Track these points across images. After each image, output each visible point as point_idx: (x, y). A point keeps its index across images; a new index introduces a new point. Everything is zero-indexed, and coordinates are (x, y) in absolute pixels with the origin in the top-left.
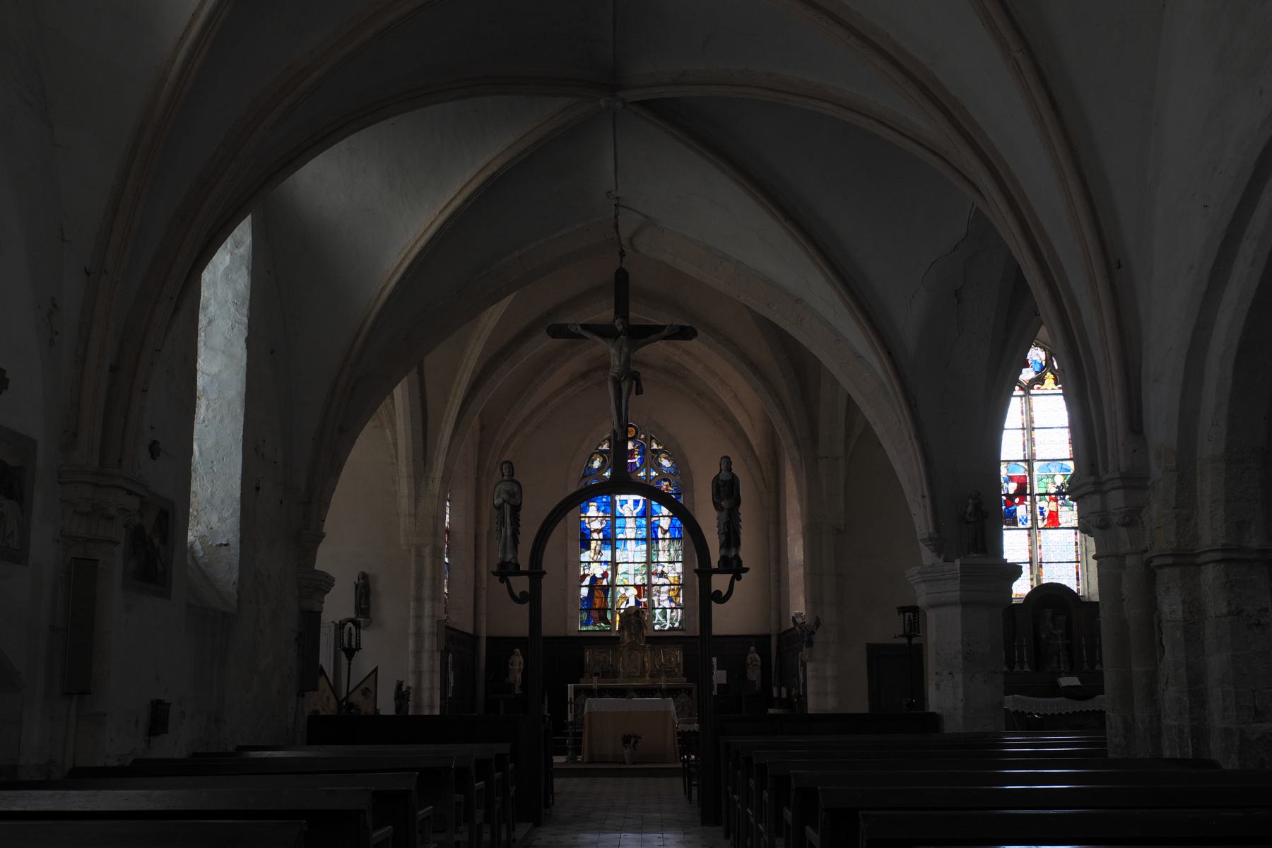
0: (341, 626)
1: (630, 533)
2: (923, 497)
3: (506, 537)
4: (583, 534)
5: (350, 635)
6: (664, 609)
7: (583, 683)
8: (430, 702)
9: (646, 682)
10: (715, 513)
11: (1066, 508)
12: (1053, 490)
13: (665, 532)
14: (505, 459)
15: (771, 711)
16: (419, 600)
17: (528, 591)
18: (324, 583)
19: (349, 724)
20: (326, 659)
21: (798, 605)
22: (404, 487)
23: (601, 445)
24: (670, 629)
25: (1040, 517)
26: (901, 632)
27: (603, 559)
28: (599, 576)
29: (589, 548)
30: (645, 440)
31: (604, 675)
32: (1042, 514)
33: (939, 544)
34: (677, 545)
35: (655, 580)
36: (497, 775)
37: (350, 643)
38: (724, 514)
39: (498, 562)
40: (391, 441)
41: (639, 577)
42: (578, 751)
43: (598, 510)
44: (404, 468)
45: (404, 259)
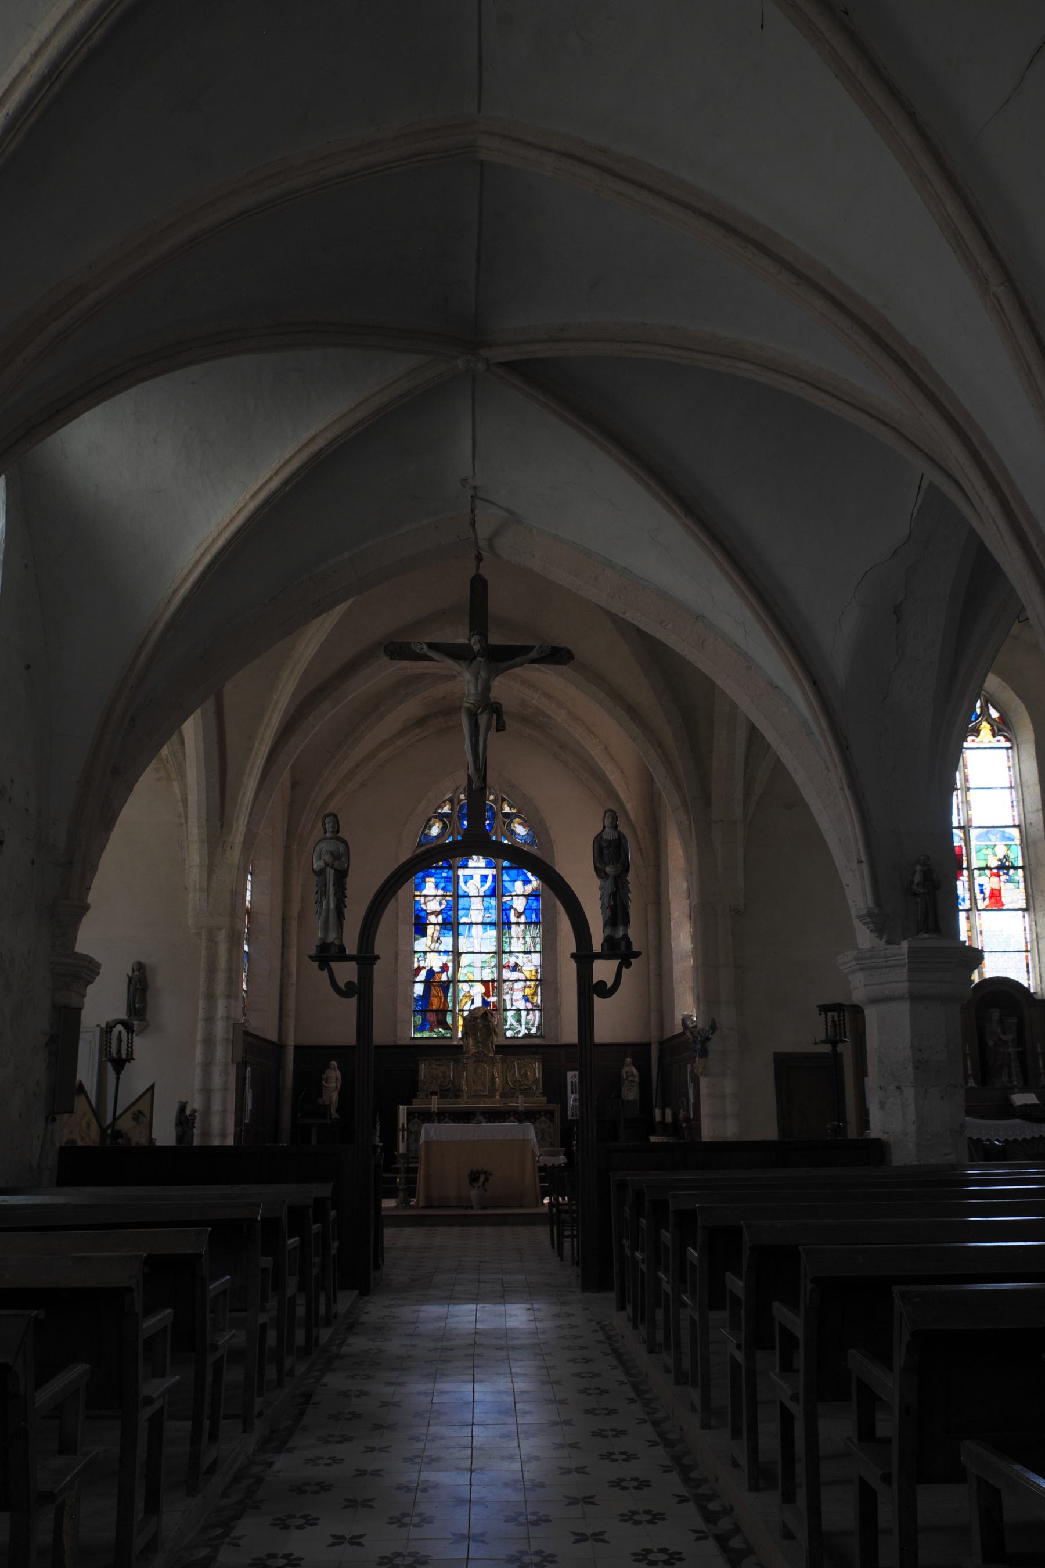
0: (109, 1028)
1: (476, 916)
2: (860, 862)
3: (328, 910)
4: (417, 917)
5: (120, 1040)
6: (518, 1010)
7: (417, 1105)
8: (221, 1129)
9: (495, 1103)
10: (597, 882)
11: (1010, 885)
12: (994, 863)
13: (519, 915)
14: (331, 808)
15: (653, 1139)
16: (210, 997)
17: (355, 981)
18: (86, 971)
19: (114, 1159)
20: (86, 1072)
21: (686, 1006)
22: (195, 855)
23: (441, 807)
24: (526, 1036)
25: (979, 896)
26: (823, 1037)
27: (442, 948)
28: (437, 969)
29: (424, 935)
30: (495, 801)
31: (443, 1094)
32: (982, 892)
33: (881, 922)
34: (534, 931)
35: (507, 974)
36: (316, 1227)
37: (119, 1051)
38: (609, 883)
39: (317, 943)
40: (179, 797)
41: (487, 971)
42: (411, 1193)
43: (437, 886)
44: (194, 830)
45: (203, 555)
